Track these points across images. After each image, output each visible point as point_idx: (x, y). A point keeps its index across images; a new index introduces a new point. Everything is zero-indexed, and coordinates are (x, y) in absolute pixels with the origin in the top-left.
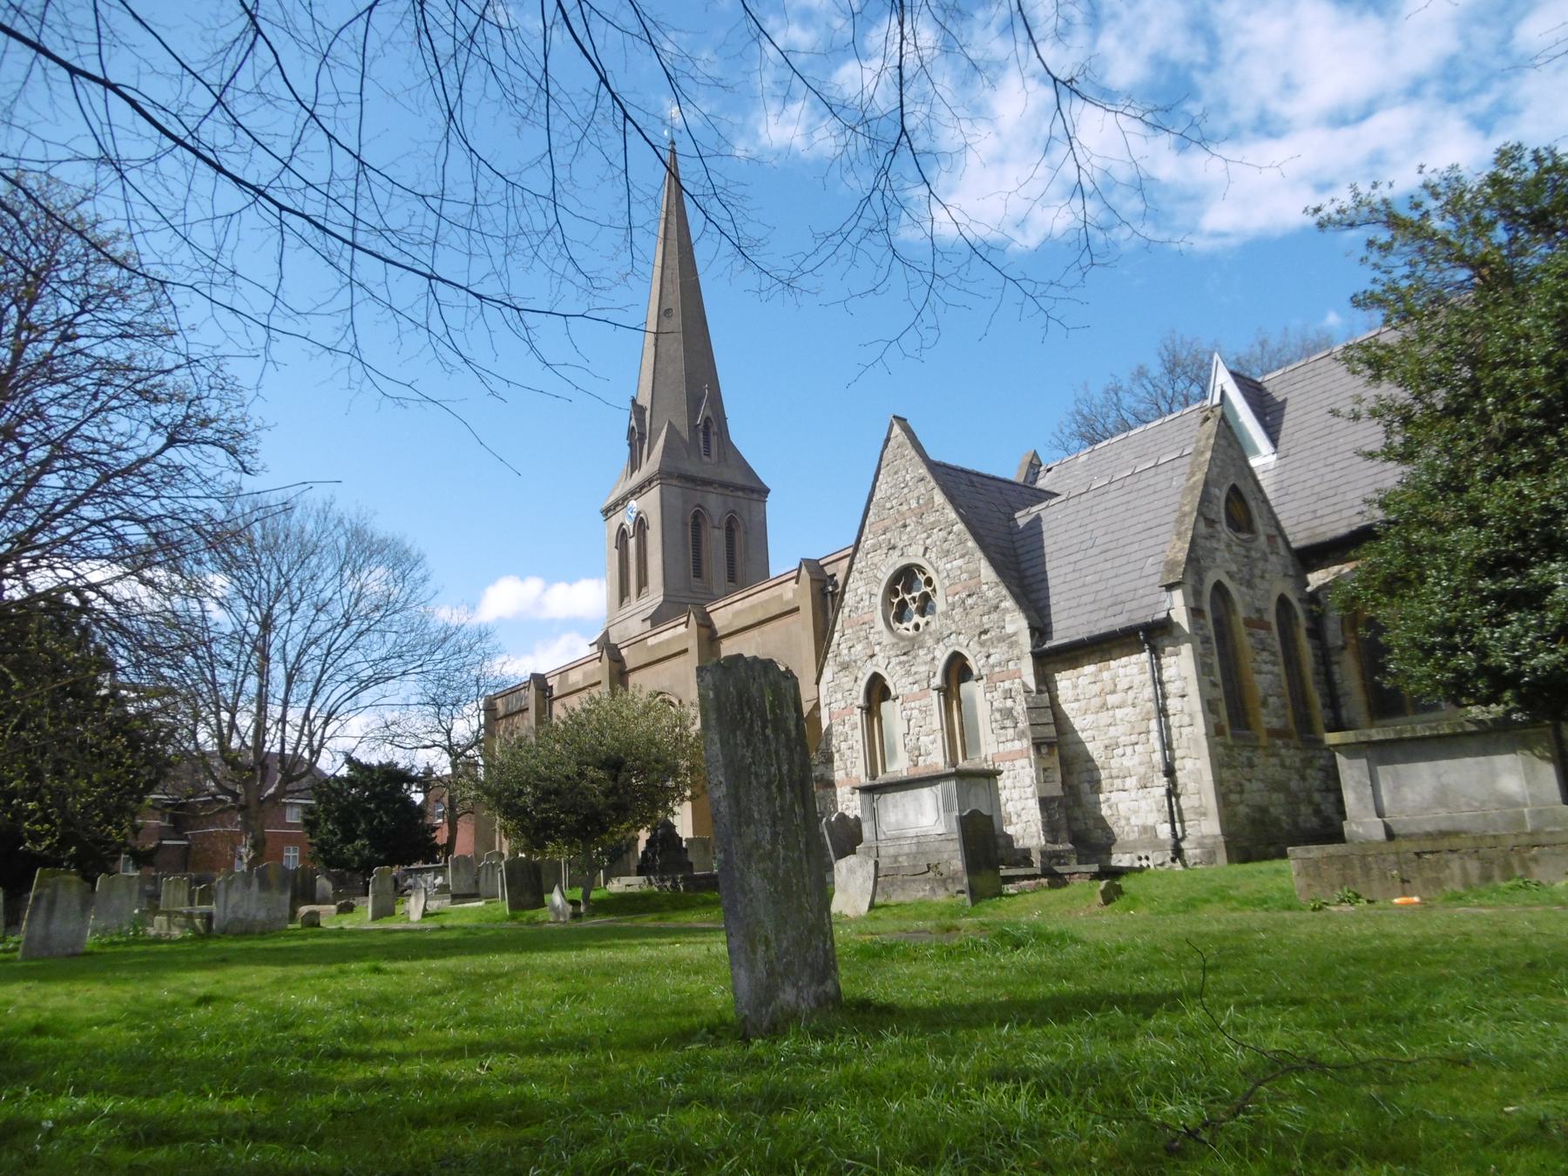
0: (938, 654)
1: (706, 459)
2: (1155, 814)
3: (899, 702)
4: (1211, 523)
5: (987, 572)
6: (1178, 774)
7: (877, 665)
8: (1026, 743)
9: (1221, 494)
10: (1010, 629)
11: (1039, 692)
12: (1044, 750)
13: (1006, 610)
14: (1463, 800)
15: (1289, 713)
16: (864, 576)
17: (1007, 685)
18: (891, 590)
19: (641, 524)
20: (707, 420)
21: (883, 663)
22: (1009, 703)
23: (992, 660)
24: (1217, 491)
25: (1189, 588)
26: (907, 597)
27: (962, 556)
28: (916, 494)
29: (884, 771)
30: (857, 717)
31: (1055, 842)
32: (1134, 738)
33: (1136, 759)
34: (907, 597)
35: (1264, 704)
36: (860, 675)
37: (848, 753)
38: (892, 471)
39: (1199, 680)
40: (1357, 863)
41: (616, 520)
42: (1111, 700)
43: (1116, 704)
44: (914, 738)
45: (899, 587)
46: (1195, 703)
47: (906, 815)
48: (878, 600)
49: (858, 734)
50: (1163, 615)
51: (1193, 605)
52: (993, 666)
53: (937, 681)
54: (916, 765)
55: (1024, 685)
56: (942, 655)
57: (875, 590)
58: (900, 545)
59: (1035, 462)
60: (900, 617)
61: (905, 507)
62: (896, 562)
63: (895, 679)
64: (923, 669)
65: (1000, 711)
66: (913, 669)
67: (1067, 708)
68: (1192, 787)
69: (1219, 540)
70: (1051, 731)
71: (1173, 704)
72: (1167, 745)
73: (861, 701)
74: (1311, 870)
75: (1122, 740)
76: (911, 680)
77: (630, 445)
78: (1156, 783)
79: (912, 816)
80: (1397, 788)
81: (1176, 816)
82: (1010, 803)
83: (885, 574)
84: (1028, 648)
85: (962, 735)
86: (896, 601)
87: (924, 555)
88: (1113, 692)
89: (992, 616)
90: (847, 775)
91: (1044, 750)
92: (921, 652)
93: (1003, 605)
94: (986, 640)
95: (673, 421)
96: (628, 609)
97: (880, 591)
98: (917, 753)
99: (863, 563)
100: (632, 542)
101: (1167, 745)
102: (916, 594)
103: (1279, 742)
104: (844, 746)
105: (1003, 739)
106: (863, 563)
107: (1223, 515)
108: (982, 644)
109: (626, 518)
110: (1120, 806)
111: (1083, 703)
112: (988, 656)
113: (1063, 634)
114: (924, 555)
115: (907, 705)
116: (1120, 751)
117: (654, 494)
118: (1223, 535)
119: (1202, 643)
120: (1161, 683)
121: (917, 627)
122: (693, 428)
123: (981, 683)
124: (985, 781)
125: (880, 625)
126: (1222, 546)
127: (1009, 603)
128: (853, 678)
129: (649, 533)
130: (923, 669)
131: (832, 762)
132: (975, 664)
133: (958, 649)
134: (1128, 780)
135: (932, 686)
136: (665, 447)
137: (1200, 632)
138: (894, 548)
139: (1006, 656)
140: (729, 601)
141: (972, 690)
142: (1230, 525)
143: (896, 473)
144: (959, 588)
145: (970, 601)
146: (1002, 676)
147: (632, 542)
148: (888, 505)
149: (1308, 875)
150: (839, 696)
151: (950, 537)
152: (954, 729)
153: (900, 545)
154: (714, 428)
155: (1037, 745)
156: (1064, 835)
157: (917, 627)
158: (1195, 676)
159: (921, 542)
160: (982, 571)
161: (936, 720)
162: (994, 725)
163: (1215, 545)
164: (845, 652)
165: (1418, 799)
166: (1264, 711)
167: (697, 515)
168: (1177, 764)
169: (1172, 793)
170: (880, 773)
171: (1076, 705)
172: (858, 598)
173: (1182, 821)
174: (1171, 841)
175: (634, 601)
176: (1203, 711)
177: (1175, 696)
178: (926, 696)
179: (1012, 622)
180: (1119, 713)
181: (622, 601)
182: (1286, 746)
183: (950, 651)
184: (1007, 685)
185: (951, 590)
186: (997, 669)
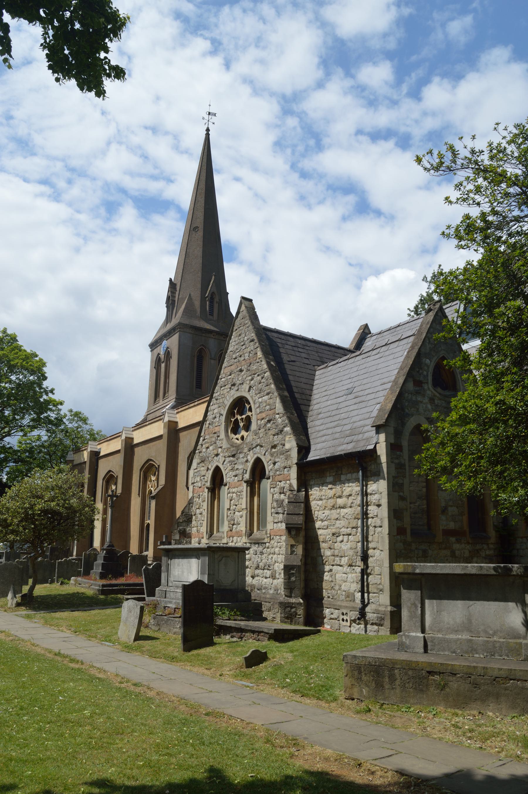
0: (249, 457)
1: (211, 317)
2: (355, 584)
3: (227, 487)
4: (418, 383)
5: (279, 407)
6: (370, 560)
7: (218, 461)
8: (283, 526)
9: (430, 363)
10: (287, 446)
11: (299, 490)
12: (293, 533)
13: (287, 433)
14: (482, 628)
15: (465, 518)
16: (218, 401)
17: (282, 484)
18: (231, 413)
19: (168, 354)
20: (212, 294)
21: (221, 461)
22: (282, 496)
23: (277, 466)
24: (428, 361)
25: (391, 430)
26: (239, 417)
27: (268, 394)
28: (249, 350)
29: (218, 531)
30: (206, 494)
31: (290, 597)
32: (349, 531)
33: (349, 545)
34: (239, 417)
35: (444, 511)
36: (210, 467)
37: (199, 516)
38: (239, 333)
39: (389, 495)
40: (387, 673)
41: (156, 351)
42: (340, 501)
43: (342, 505)
44: (232, 512)
45: (236, 411)
46: (384, 512)
47: (183, 572)
48: (223, 418)
49: (205, 505)
50: (371, 447)
51: (392, 441)
52: (276, 471)
53: (247, 476)
54: (231, 531)
55: (291, 485)
56: (251, 458)
57: (222, 412)
58: (238, 382)
59: (366, 331)
60: (235, 431)
61: (242, 358)
62: (234, 394)
63: (226, 471)
64: (240, 467)
65: (277, 501)
66: (236, 466)
67: (314, 504)
68: (377, 570)
69: (424, 396)
70: (300, 520)
71: (372, 510)
72: (365, 538)
73: (208, 484)
74: (356, 673)
75: (344, 531)
76: (234, 473)
77: (167, 307)
78: (357, 564)
79: (185, 574)
80: (439, 611)
81: (366, 589)
82: (277, 564)
83: (228, 402)
84: (295, 461)
85: (258, 514)
86: (233, 420)
87: (249, 391)
88: (340, 497)
89: (279, 436)
90: (198, 531)
91: (293, 533)
92: (241, 456)
93: (285, 429)
94: (274, 452)
95: (192, 294)
96: (158, 405)
97: (224, 413)
98: (232, 522)
99: (218, 393)
100: (163, 365)
101: (365, 538)
102: (244, 416)
103: (453, 539)
104: (198, 511)
105: (276, 521)
106: (218, 393)
107: (430, 378)
108: (272, 455)
109: (161, 350)
110: (337, 576)
111: (324, 501)
112: (274, 464)
113: (318, 452)
114: (249, 391)
115: (231, 490)
116: (340, 538)
117: (175, 338)
118: (428, 392)
119: (396, 468)
120: (367, 494)
121: (242, 438)
122: (203, 299)
123: (269, 481)
124: (235, 554)
125: (222, 435)
126: (426, 400)
127: (288, 429)
128: (206, 468)
129: (171, 361)
130: (240, 467)
131: (191, 521)
132: (268, 467)
133: (259, 456)
134: (343, 559)
135: (245, 479)
136: (185, 309)
137: (397, 461)
138: (234, 385)
139: (283, 465)
140: (187, 407)
141: (266, 484)
142: (435, 384)
143: (240, 335)
144: (264, 415)
145: (269, 425)
146: (280, 478)
147: (163, 365)
148: (234, 356)
149: (353, 676)
150: (198, 479)
151: (263, 380)
152: (253, 509)
153: (238, 382)
154: (217, 299)
155: (289, 529)
156: (297, 592)
157: (242, 438)
158: (386, 493)
159: (248, 382)
160: (277, 405)
161: (244, 503)
162: (273, 510)
163: (419, 398)
164: (204, 450)
165: (452, 622)
166: (443, 518)
167: (201, 351)
168: (370, 552)
169: (365, 573)
170: (215, 532)
171: (320, 503)
172: (214, 416)
173: (368, 593)
174: (360, 606)
175: (161, 401)
176: (389, 517)
177: (374, 504)
178: (240, 485)
179: (289, 441)
180: (343, 511)
181: (155, 399)
182: (458, 541)
183: (255, 456)
184: (282, 484)
185: (260, 416)
186: (278, 473)
